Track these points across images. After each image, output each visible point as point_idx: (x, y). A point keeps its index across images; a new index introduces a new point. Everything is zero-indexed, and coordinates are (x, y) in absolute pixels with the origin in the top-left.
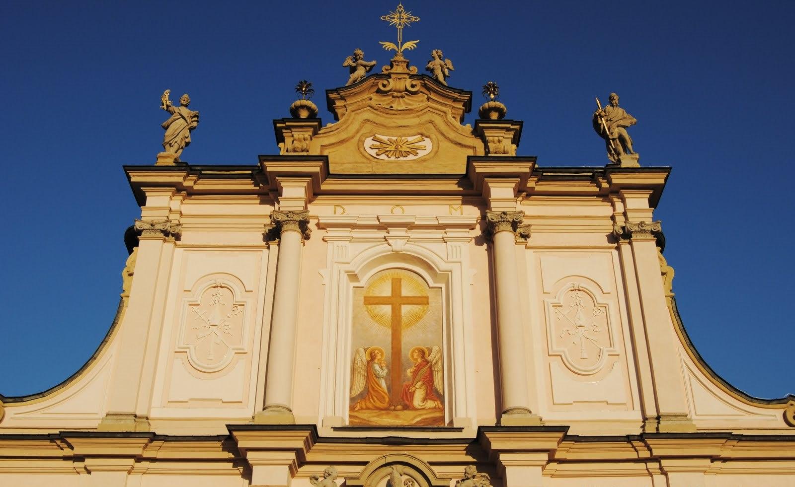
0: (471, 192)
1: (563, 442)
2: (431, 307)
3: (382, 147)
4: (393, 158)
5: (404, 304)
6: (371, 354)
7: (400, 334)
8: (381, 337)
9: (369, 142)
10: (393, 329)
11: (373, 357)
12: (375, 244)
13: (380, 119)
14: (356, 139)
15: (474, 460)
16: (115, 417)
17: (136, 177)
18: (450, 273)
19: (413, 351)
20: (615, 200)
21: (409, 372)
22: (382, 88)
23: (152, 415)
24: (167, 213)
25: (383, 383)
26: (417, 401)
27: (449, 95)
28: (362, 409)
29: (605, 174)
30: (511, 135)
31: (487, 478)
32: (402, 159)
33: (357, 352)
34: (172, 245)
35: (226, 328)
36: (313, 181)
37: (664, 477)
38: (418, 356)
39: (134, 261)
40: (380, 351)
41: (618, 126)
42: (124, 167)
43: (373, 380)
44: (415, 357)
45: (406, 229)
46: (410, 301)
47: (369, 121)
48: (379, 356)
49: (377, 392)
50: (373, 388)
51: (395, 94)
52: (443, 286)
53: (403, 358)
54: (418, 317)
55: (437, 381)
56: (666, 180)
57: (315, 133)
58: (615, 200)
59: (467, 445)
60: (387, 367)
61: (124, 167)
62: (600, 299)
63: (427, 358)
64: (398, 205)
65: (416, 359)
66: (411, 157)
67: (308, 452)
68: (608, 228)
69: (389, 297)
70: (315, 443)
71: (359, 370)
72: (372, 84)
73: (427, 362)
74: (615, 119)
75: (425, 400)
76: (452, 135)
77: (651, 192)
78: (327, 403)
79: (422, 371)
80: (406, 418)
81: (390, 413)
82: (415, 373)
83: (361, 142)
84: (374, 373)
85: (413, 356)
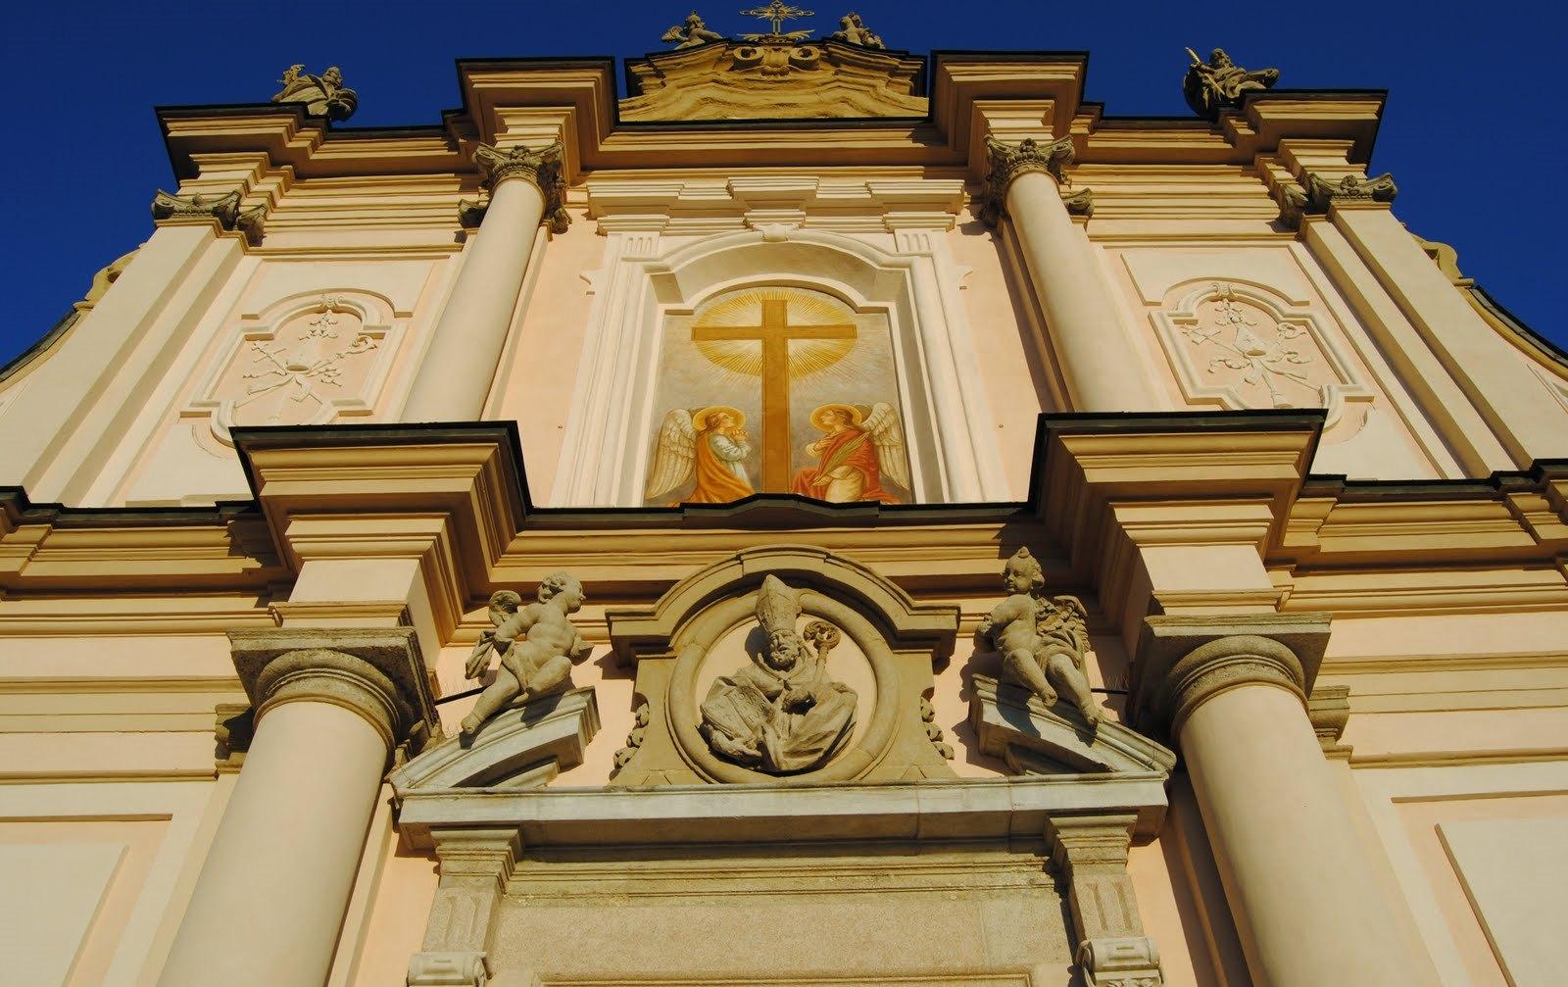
1: (1301, 500)
7: (786, 384)
8: (738, 392)
10: (766, 377)
17: (179, 129)
18: (907, 270)
27: (879, 63)
29: (1241, 108)
31: (1076, 609)
35: (330, 373)
36: (578, 113)
39: (131, 259)
42: (157, 109)
43: (710, 465)
45: (797, 212)
49: (722, 486)
50: (710, 481)
52: (892, 307)
55: (889, 463)
56: (1379, 113)
59: (1001, 526)
60: (749, 441)
61: (157, 109)
63: (859, 424)
67: (495, 560)
68: (1273, 211)
70: (519, 531)
72: (721, 55)
73: (861, 431)
79: (846, 447)
84: (714, 453)
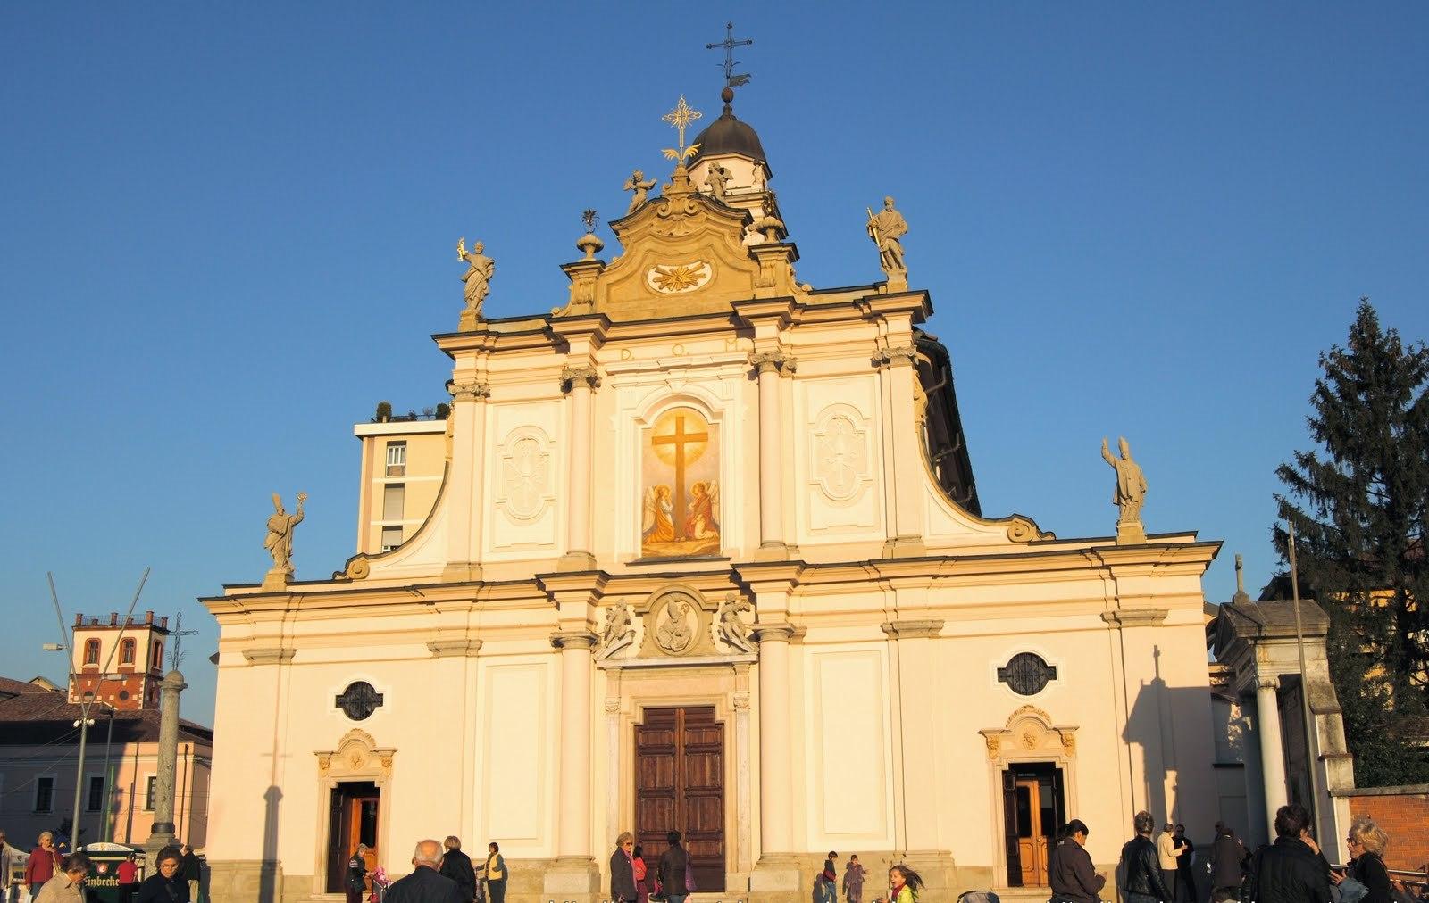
0: (741, 327)
3: (664, 280)
4: (675, 291)
6: (659, 491)
7: (683, 470)
8: (667, 474)
9: (652, 274)
11: (660, 494)
12: (657, 387)
13: (661, 248)
14: (640, 272)
15: (737, 586)
16: (453, 566)
19: (695, 487)
20: (879, 321)
21: (691, 507)
22: (662, 214)
23: (485, 559)
24: (474, 374)
25: (669, 518)
26: (698, 533)
30: (784, 256)
32: (683, 291)
34: (483, 404)
37: (1113, 582)
40: (667, 488)
41: (888, 237)
47: (651, 250)
48: (665, 493)
51: (675, 217)
53: (686, 494)
54: (698, 454)
57: (600, 272)
58: (879, 321)
60: (672, 502)
62: (859, 427)
64: (678, 344)
66: (692, 288)
73: (706, 496)
74: (886, 230)
75: (704, 531)
76: (730, 259)
77: (912, 313)
78: (620, 543)
80: (689, 548)
82: (696, 507)
83: (645, 275)
85: (694, 491)
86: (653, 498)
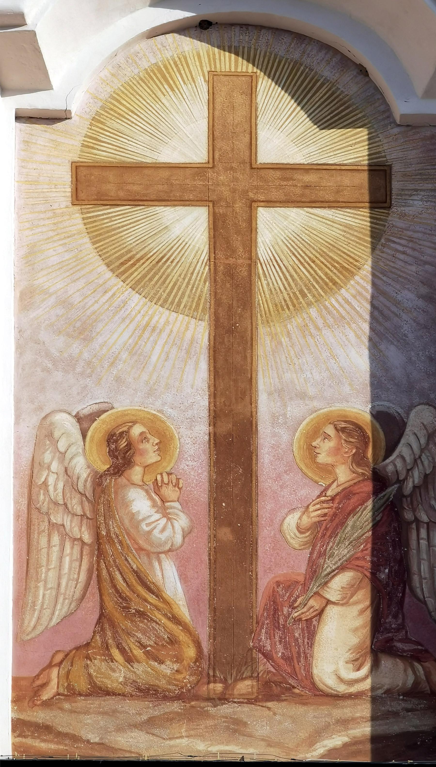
2: (403, 216)
5: (270, 203)
6: (111, 438)
11: (120, 452)
19: (315, 432)
28: (72, 693)
33: (46, 434)
38: (337, 451)
44: (322, 458)
46: (231, 238)
65: (327, 470)
69: (199, 170)
71: (58, 518)
81: (205, 715)
86: (81, 467)
